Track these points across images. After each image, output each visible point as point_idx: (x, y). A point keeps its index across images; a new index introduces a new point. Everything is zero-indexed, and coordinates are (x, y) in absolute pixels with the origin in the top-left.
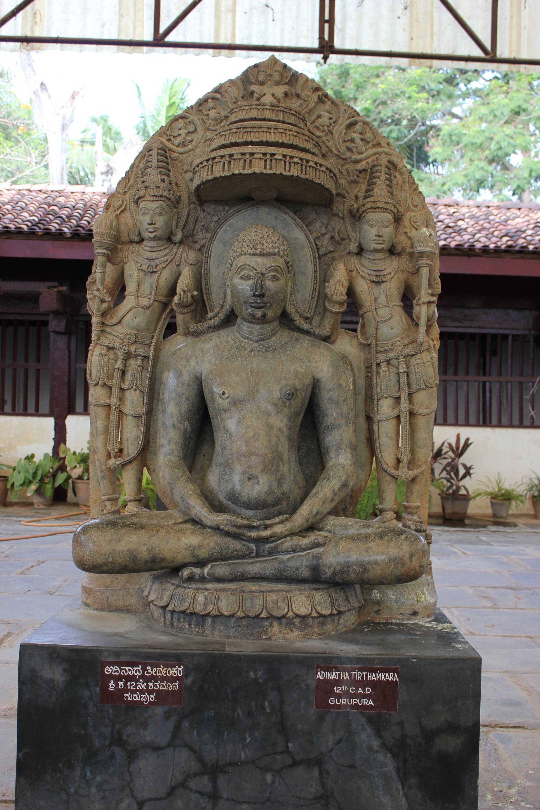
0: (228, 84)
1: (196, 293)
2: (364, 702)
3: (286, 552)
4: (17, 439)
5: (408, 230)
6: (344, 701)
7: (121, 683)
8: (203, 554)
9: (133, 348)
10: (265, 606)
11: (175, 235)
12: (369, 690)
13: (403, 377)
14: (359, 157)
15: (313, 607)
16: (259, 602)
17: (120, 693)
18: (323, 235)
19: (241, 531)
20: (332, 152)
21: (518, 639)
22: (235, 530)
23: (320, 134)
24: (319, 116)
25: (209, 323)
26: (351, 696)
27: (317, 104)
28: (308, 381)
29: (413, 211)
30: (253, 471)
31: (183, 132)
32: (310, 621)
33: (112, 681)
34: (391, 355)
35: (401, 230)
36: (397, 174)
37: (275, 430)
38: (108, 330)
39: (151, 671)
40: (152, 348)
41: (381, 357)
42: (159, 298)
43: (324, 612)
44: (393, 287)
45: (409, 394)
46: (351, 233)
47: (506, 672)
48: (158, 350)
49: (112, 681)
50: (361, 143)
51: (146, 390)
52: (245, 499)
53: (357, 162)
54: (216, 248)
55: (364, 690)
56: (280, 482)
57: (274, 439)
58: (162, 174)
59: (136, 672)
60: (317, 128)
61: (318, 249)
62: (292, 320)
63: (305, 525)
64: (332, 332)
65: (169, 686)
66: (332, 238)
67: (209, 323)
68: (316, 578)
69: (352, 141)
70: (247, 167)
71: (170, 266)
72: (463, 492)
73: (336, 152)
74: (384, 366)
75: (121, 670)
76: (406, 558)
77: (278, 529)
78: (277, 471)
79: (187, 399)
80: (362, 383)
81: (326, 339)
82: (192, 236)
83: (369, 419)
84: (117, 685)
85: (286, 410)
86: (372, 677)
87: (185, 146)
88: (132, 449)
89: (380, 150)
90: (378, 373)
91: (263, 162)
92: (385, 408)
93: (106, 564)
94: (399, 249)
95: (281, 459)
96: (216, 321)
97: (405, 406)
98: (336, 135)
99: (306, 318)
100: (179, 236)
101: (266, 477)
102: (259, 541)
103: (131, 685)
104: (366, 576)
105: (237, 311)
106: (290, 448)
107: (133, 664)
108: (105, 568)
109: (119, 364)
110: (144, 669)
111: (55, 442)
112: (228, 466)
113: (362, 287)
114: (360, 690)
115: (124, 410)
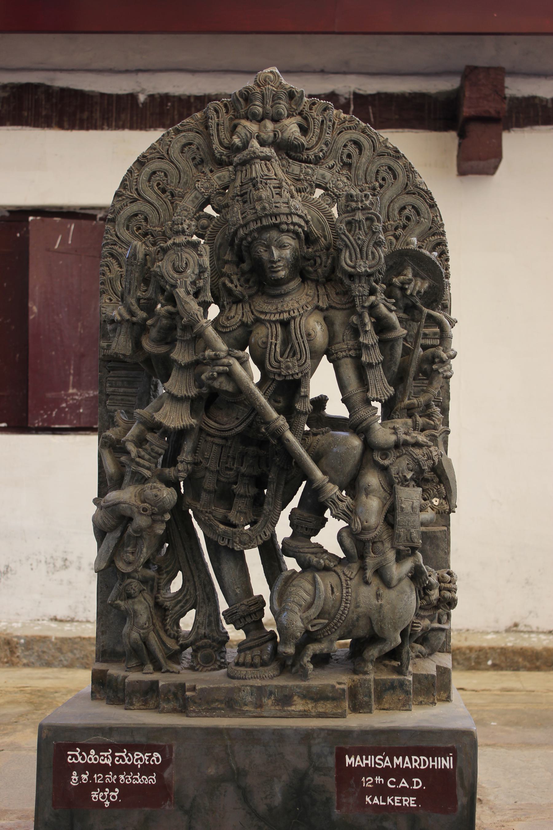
0: (446, 680)
7: (84, 777)
12: (418, 784)
21: (489, 742)
33: (75, 773)
49: (75, 773)
55: (411, 783)
59: (137, 761)
65: (144, 779)
84: (80, 779)
103: (98, 778)
111: (159, 127)
114: (404, 783)
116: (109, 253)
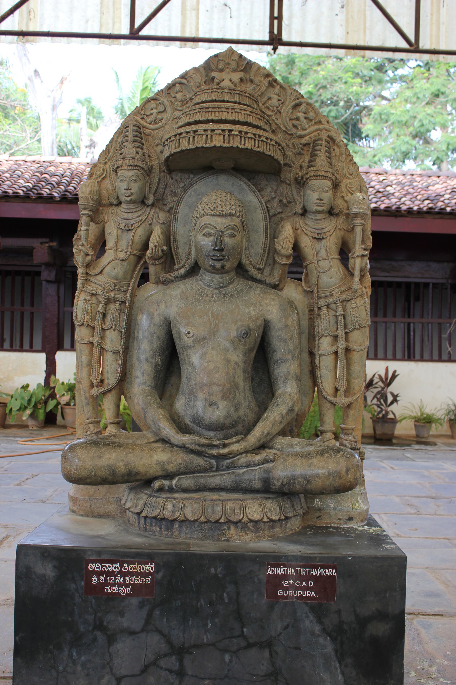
1: (165, 248)
2: (308, 593)
3: (241, 467)
4: (15, 371)
5: (344, 194)
6: (290, 593)
7: (102, 578)
8: (171, 468)
9: (112, 295)
10: (223, 512)
11: (148, 199)
12: (311, 584)
13: (340, 319)
14: (303, 133)
15: (265, 513)
16: (219, 509)
17: (102, 586)
18: (273, 199)
19: (204, 449)
20: (280, 128)
22: (198, 448)
23: (270, 113)
24: (270, 99)
25: (176, 273)
26: (297, 589)
27: (267, 88)
28: (260, 322)
29: (349, 178)
30: (214, 399)
31: (155, 111)
32: (262, 525)
33: (95, 576)
34: (330, 300)
35: (339, 195)
36: (335, 147)
37: (232, 363)
38: (91, 279)
39: (128, 568)
40: (128, 294)
41: (322, 302)
42: (134, 252)
43: (274, 518)
44: (332, 243)
45: (346, 333)
46: (296, 197)
47: (427, 568)
48: (133, 296)
49: (95, 576)
50: (305, 121)
51: (123, 330)
52: (207, 422)
53: (301, 137)
54: (183, 210)
55: (308, 584)
56: (237, 408)
57: (231, 371)
58: (137, 147)
59: (115, 568)
60: (268, 108)
61: (268, 211)
62: (247, 271)
63: (257, 444)
64: (280, 281)
65: (143, 580)
66: (281, 201)
67: (176, 273)
68: (267, 489)
69: (298, 119)
70: (209, 141)
71: (143, 225)
72: (391, 416)
73: (284, 129)
74: (324, 310)
75: (102, 566)
76: (343, 472)
77: (235, 448)
78: (234, 398)
79: (158, 337)
80: (305, 323)
81: (275, 287)
82: (163, 199)
83: (312, 354)
84: (99, 579)
85: (242, 347)
86: (314, 572)
87: (156, 123)
88: (111, 380)
89: (321, 126)
90: (319, 315)
91: (222, 137)
92: (325, 345)
93: (90, 477)
94: (337, 210)
95: (238, 388)
96: (183, 271)
97: (342, 343)
98: (284, 114)
99: (259, 269)
100: (151, 200)
101: (225, 403)
102: (218, 457)
103: (110, 579)
104: (309, 487)
105: (200, 263)
106: (245, 379)
107: (112, 562)
108: (88, 480)
109: (100, 308)
110: (122, 566)
112: (192, 394)
113: (306, 243)
114: (304, 584)
115: (105, 347)
116: (147, 87)
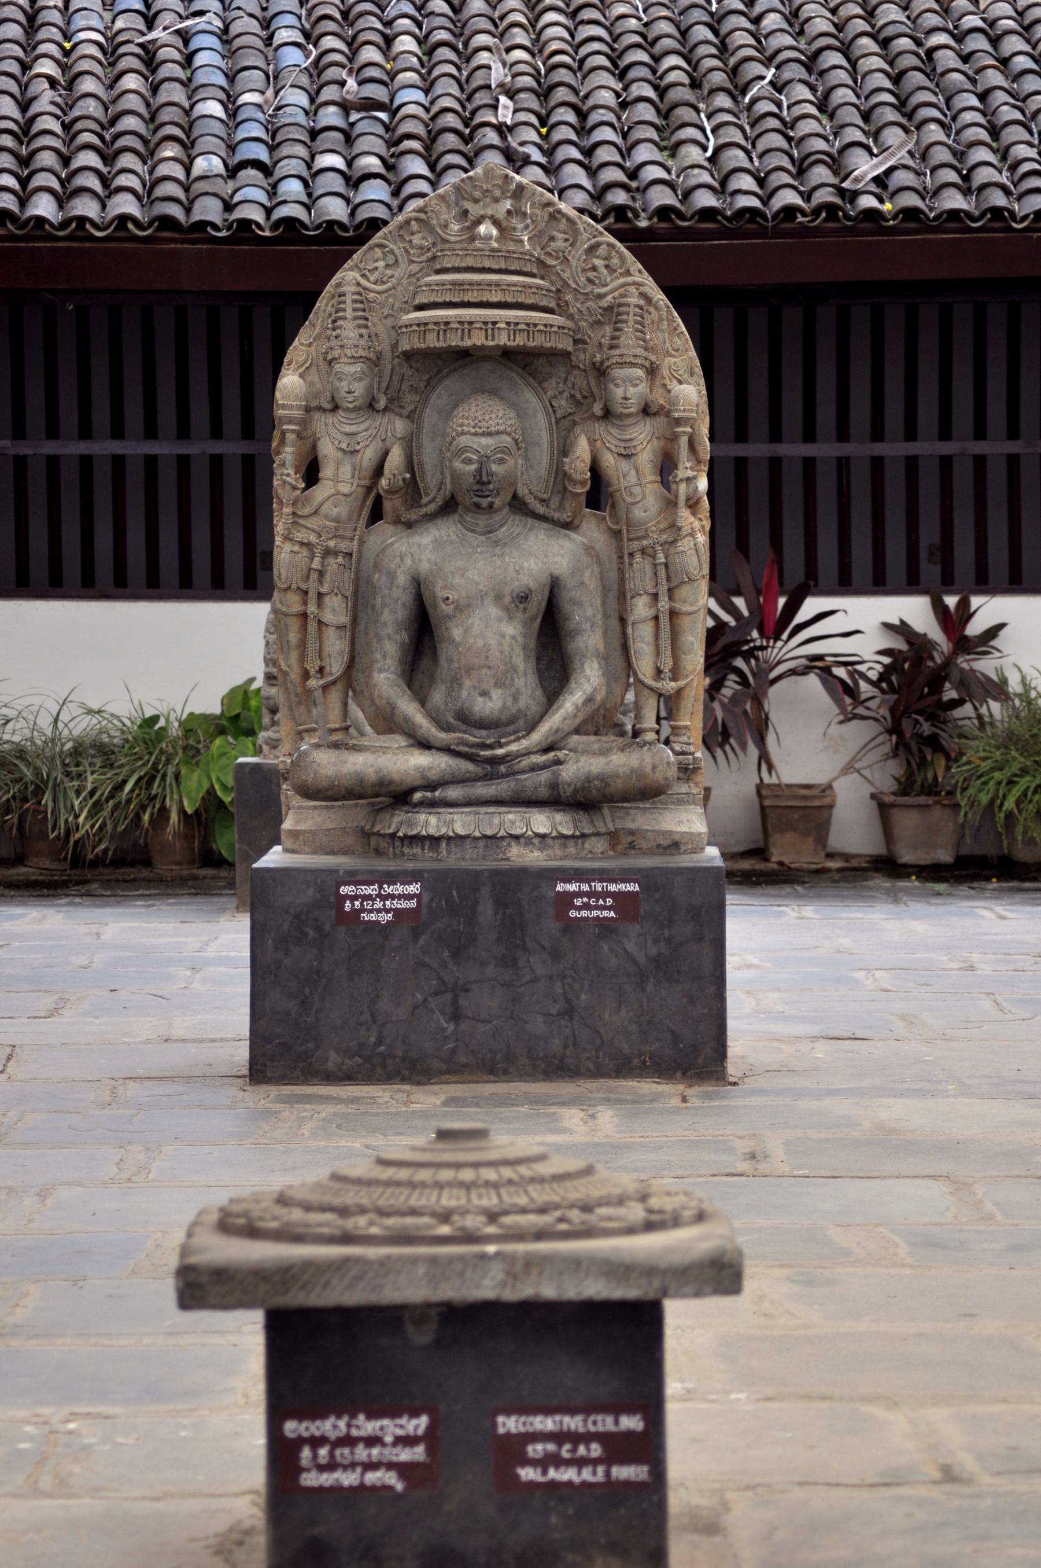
1: (408, 476)
2: (606, 914)
3: (522, 772)
5: (667, 381)
6: (584, 913)
7: (357, 903)
8: (433, 775)
9: (331, 544)
10: (501, 825)
11: (378, 402)
13: (662, 572)
14: (603, 290)
15: (554, 827)
16: (496, 821)
17: (356, 913)
18: (561, 393)
19: (473, 751)
20: (569, 286)
22: (466, 749)
23: (553, 262)
24: (552, 239)
25: (424, 510)
27: (548, 222)
28: (545, 579)
29: (671, 356)
30: (485, 686)
31: (381, 264)
32: (550, 841)
34: (645, 543)
35: (658, 383)
36: (652, 310)
37: (508, 638)
38: (301, 521)
39: (388, 889)
40: (355, 543)
41: (635, 545)
42: (362, 482)
43: (565, 832)
44: (646, 457)
45: (669, 590)
46: (595, 390)
48: (362, 542)
50: (605, 272)
51: (349, 593)
52: (477, 717)
53: (601, 296)
54: (429, 417)
56: (515, 699)
57: (506, 649)
58: (359, 327)
60: (549, 254)
61: (554, 412)
62: (525, 504)
63: (544, 745)
64: (574, 516)
66: (572, 396)
67: (424, 510)
68: (553, 800)
69: (594, 269)
70: (466, 338)
71: (374, 442)
73: (574, 286)
74: (638, 558)
76: (648, 770)
77: (514, 747)
78: (512, 685)
79: (404, 604)
80: (613, 576)
81: (568, 526)
82: (398, 399)
83: (623, 621)
85: (520, 615)
86: (612, 888)
87: (384, 283)
88: (336, 668)
89: (629, 279)
90: (631, 565)
91: (483, 332)
92: (641, 608)
93: (331, 787)
94: (654, 409)
95: (516, 671)
96: (432, 508)
97: (664, 604)
98: (573, 263)
99: (542, 501)
100: (382, 403)
101: (500, 692)
102: (494, 761)
104: (608, 791)
105: (459, 498)
106: (527, 658)
107: (369, 883)
108: (330, 793)
109: (316, 564)
110: (380, 888)
112: (456, 682)
113: (609, 461)
114: (601, 902)
115: (324, 620)
